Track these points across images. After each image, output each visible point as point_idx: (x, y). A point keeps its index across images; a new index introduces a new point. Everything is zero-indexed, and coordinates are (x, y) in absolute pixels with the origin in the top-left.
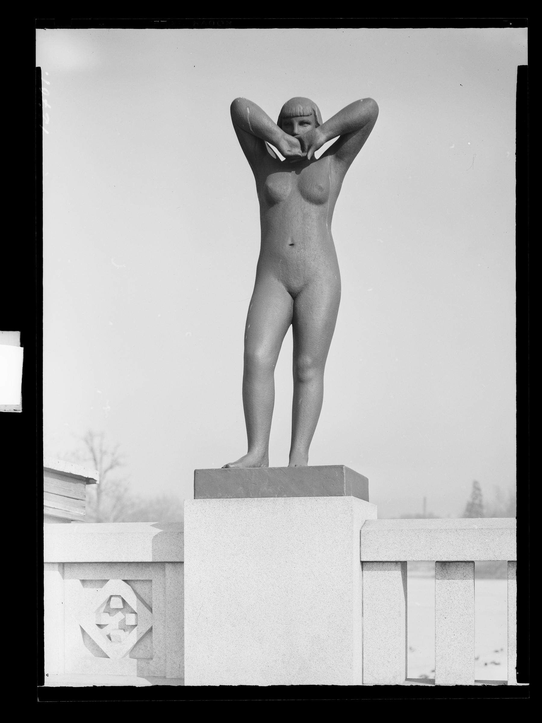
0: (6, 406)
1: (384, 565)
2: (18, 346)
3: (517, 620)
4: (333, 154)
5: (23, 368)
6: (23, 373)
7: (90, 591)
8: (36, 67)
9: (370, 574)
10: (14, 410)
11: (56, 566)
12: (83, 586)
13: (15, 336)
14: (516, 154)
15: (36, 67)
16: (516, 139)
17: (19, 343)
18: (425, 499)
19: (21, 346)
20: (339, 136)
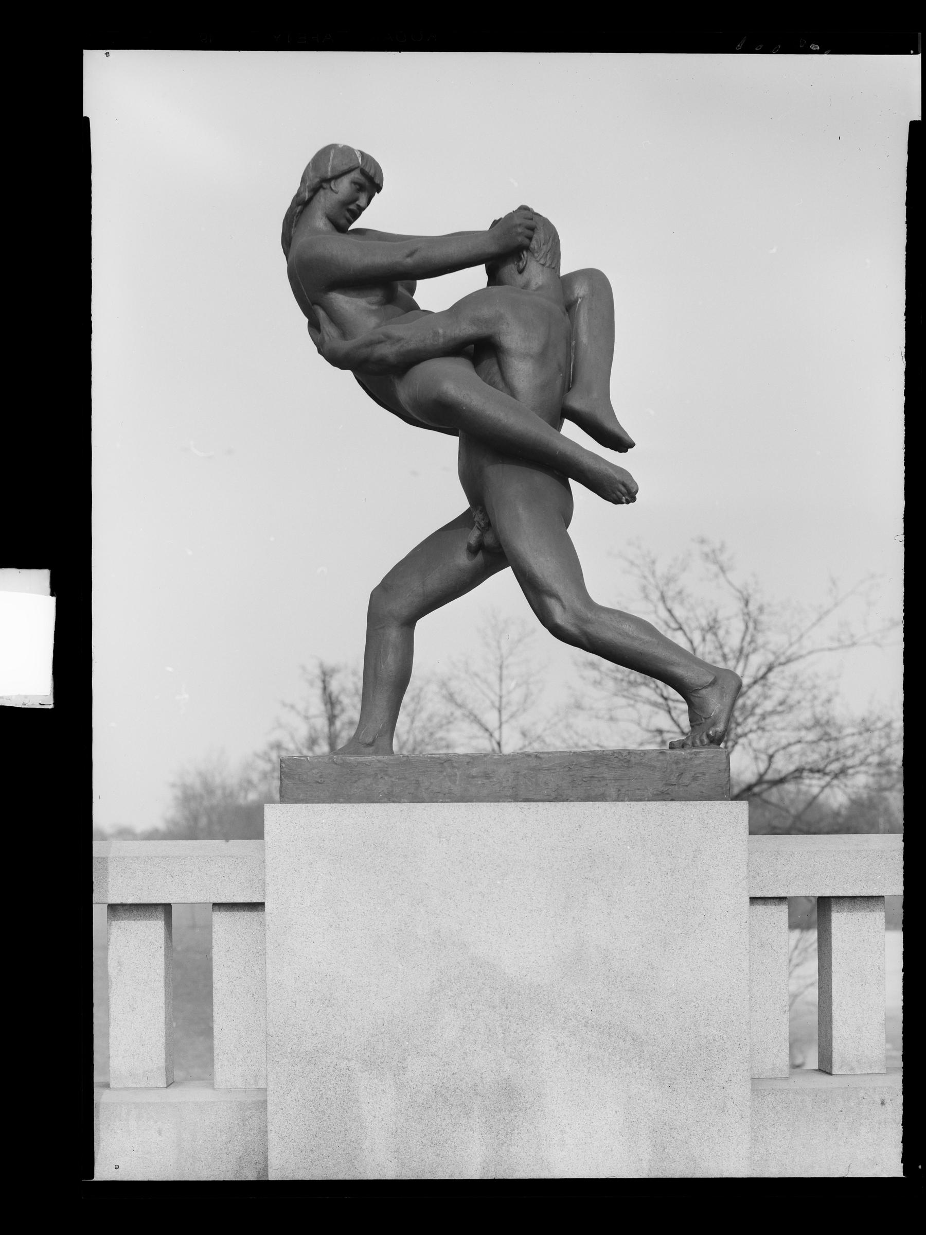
0: (26, 697)
2: (47, 595)
3: (906, 251)
4: (830, 911)
5: (55, 632)
6: (55, 641)
8: (917, 58)
10: (40, 704)
13: (42, 577)
14: (905, 478)
16: (907, 261)
17: (48, 590)
18: (753, 900)
19: (52, 595)
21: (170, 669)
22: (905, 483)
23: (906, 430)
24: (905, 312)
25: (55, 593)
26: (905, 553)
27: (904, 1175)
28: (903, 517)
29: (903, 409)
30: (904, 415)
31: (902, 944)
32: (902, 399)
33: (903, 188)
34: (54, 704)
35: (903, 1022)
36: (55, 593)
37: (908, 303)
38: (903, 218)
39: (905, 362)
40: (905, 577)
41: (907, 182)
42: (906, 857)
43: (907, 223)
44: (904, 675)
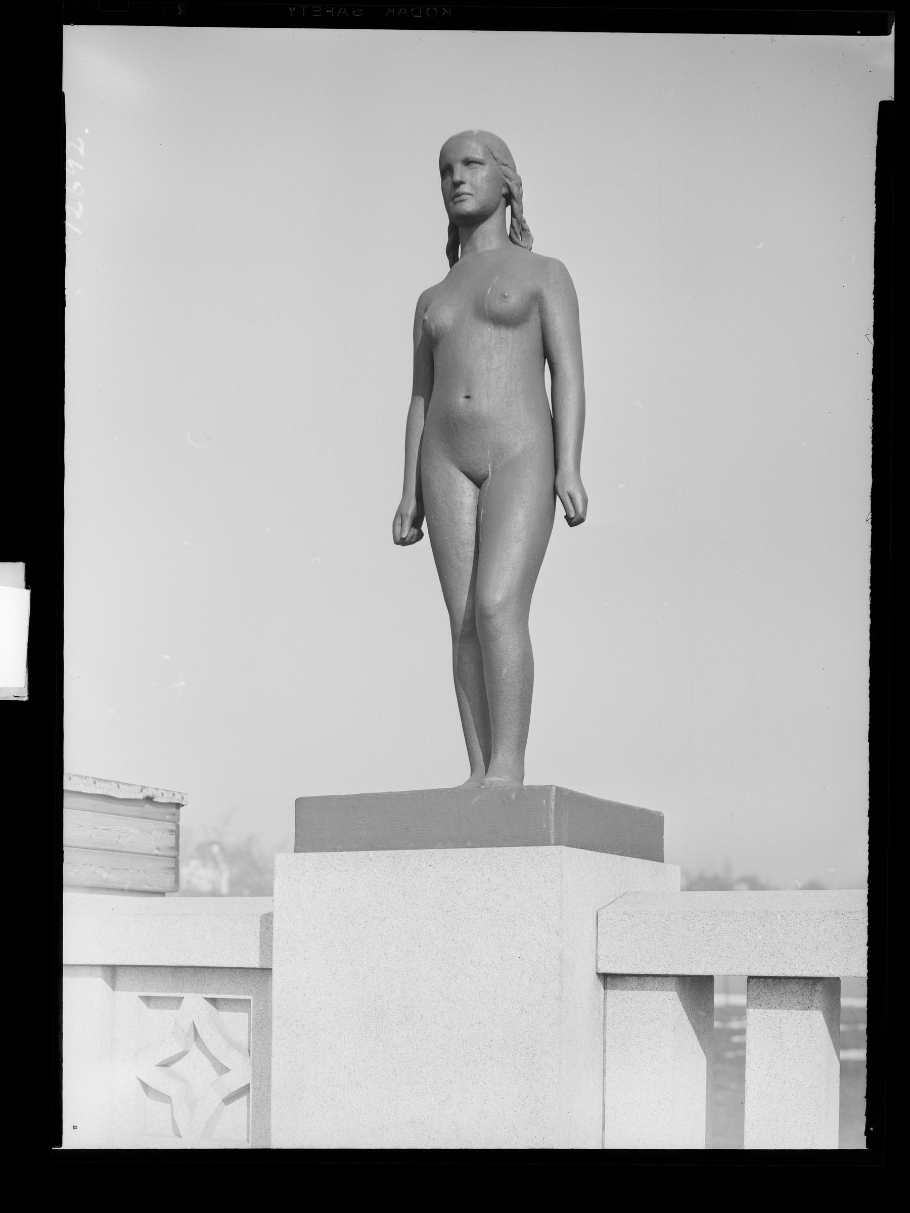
1: (208, 970)
3: (875, 230)
7: (154, 1014)
8: (888, 42)
9: (615, 995)
10: (15, 696)
11: (674, 981)
12: (148, 1006)
13: (17, 570)
15: (888, 42)
16: (875, 241)
17: (23, 584)
19: (27, 588)
20: (546, 360)
21: (167, 657)
22: (872, 461)
23: (873, 409)
24: (870, 694)
25: (29, 586)
26: (870, 696)
27: (867, 1147)
28: (870, 494)
29: (871, 387)
30: (874, 187)
31: (868, 612)
32: (871, 378)
33: (867, 728)
34: (28, 696)
35: (876, 162)
36: (29, 586)
37: (876, 282)
38: (873, 198)
39: (872, 341)
40: (872, 533)
41: (873, 385)
42: (871, 832)
43: (876, 202)
44: (870, 651)
